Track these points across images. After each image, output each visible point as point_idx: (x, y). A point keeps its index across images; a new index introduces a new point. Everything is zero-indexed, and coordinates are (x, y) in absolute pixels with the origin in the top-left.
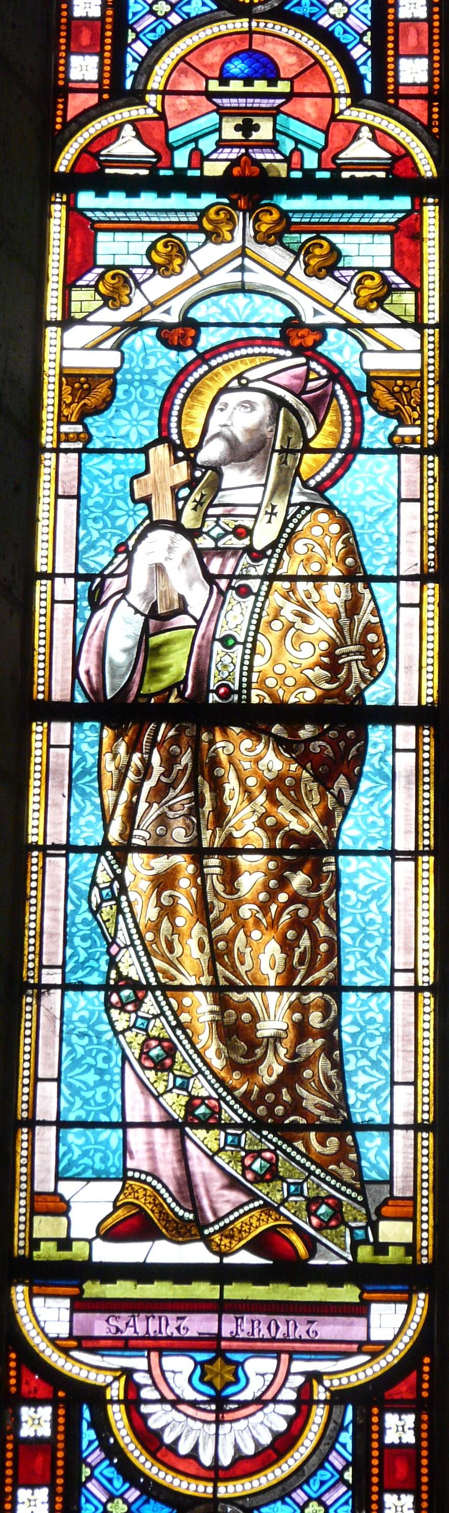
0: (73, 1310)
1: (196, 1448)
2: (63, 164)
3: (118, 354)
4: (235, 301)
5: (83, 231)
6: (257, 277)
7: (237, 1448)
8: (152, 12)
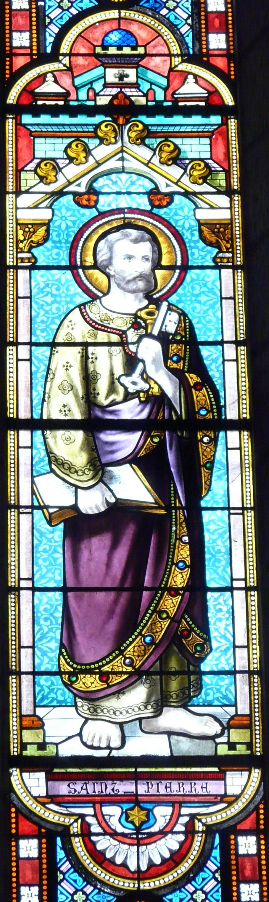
0: (48, 779)
2: (12, 98)
3: (50, 210)
6: (131, 164)
7: (150, 860)
8: (60, 7)
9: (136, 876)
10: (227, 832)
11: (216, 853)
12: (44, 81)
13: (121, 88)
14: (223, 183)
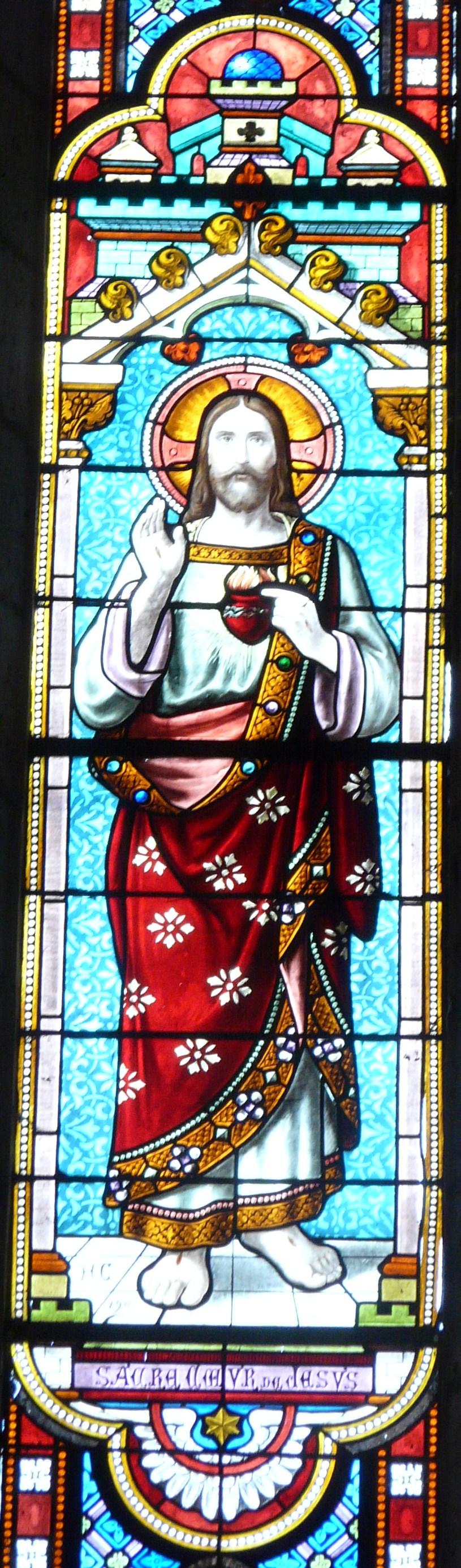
1: (198, 1501)
2: (63, 170)
4: (240, 316)
5: (83, 237)
6: (262, 289)
9: (216, 1528)
10: (372, 1458)
11: (353, 1490)
12: (119, 140)
13: (251, 153)
14: (418, 325)
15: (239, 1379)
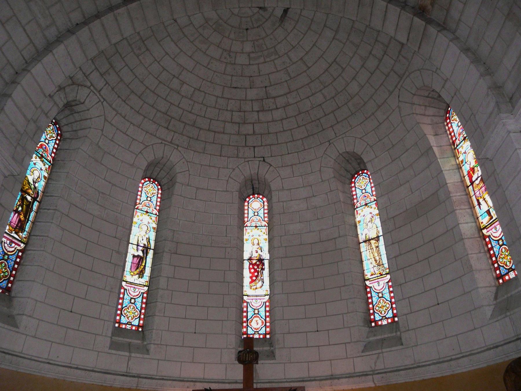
15: (257, 298)
